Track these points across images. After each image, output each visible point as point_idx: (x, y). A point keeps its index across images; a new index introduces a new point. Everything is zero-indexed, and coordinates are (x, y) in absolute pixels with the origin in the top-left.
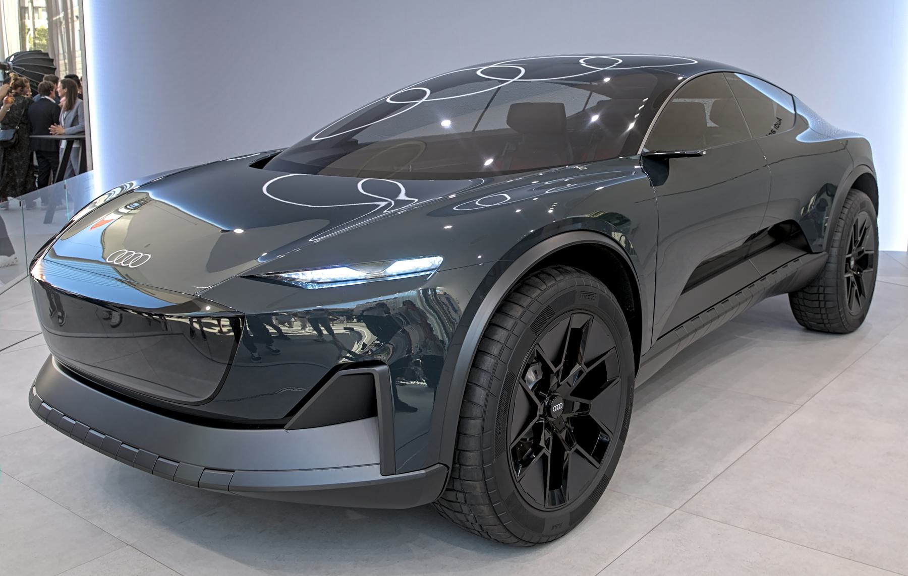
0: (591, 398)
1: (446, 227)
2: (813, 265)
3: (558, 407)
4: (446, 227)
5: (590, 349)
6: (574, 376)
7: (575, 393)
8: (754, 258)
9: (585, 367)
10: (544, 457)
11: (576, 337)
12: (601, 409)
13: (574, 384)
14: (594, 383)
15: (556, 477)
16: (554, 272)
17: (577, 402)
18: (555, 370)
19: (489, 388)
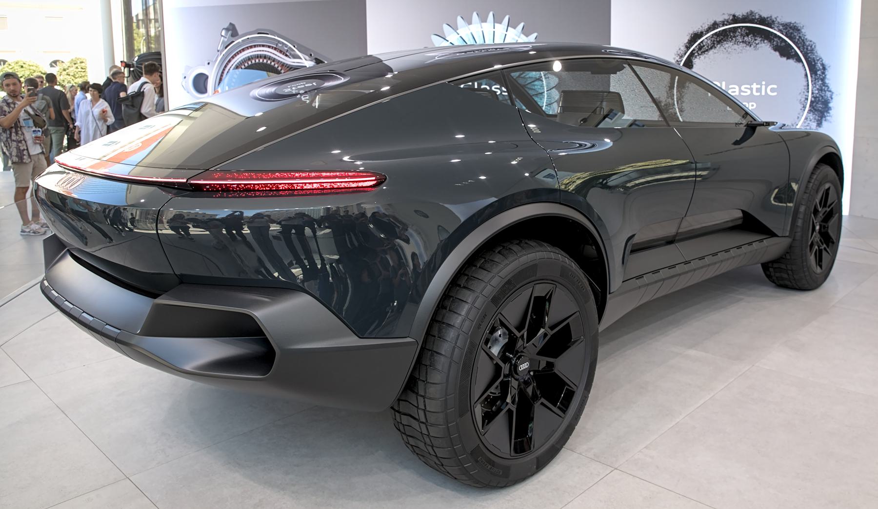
0: (556, 356)
1: (264, 128)
2: (776, 226)
3: (524, 366)
4: (264, 128)
5: (555, 313)
6: (540, 338)
7: (540, 353)
8: (682, 243)
9: (549, 330)
10: (510, 412)
11: (540, 305)
12: (566, 366)
13: (540, 346)
14: (561, 341)
15: (521, 441)
16: (515, 248)
17: (543, 361)
18: (518, 334)
19: (451, 357)
